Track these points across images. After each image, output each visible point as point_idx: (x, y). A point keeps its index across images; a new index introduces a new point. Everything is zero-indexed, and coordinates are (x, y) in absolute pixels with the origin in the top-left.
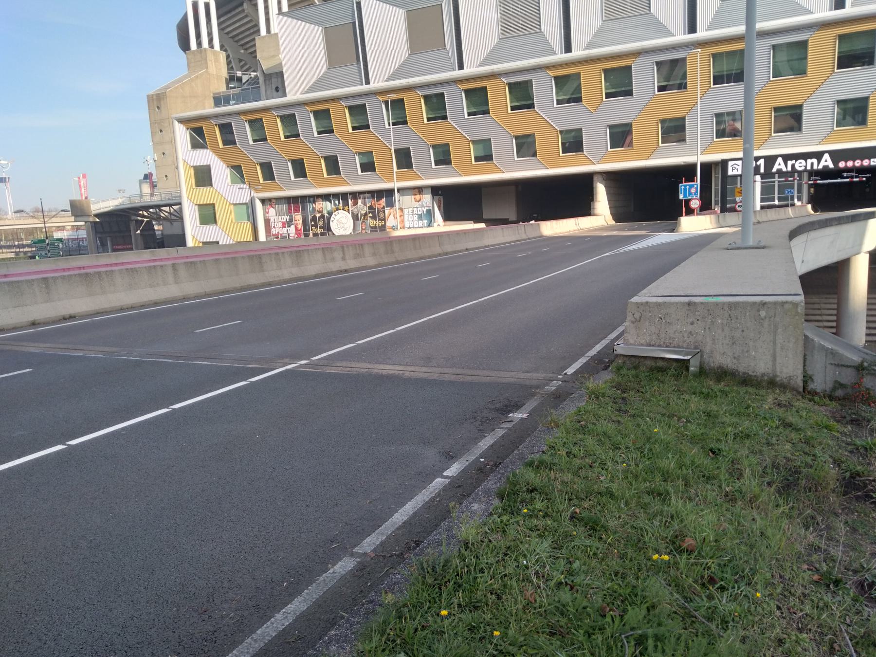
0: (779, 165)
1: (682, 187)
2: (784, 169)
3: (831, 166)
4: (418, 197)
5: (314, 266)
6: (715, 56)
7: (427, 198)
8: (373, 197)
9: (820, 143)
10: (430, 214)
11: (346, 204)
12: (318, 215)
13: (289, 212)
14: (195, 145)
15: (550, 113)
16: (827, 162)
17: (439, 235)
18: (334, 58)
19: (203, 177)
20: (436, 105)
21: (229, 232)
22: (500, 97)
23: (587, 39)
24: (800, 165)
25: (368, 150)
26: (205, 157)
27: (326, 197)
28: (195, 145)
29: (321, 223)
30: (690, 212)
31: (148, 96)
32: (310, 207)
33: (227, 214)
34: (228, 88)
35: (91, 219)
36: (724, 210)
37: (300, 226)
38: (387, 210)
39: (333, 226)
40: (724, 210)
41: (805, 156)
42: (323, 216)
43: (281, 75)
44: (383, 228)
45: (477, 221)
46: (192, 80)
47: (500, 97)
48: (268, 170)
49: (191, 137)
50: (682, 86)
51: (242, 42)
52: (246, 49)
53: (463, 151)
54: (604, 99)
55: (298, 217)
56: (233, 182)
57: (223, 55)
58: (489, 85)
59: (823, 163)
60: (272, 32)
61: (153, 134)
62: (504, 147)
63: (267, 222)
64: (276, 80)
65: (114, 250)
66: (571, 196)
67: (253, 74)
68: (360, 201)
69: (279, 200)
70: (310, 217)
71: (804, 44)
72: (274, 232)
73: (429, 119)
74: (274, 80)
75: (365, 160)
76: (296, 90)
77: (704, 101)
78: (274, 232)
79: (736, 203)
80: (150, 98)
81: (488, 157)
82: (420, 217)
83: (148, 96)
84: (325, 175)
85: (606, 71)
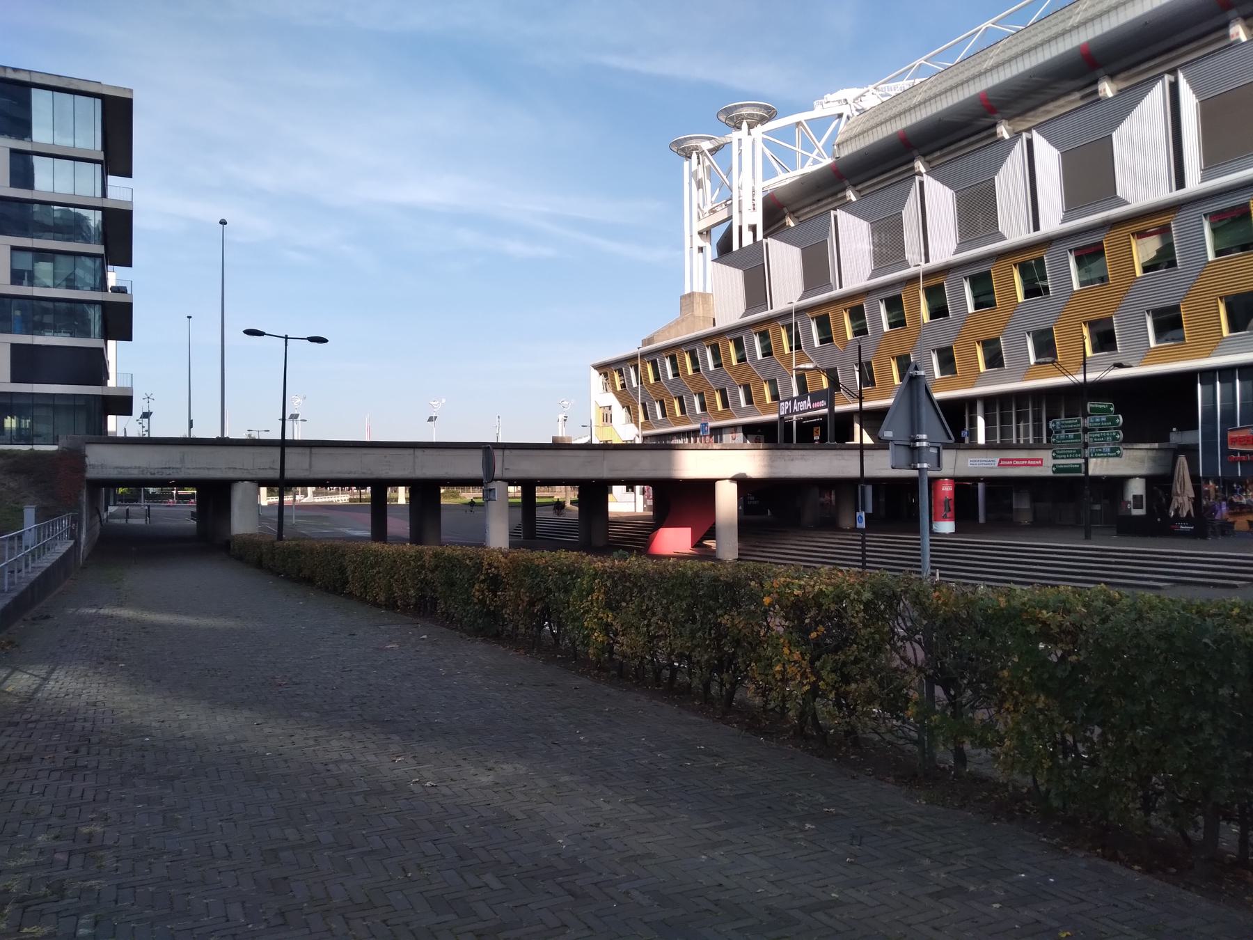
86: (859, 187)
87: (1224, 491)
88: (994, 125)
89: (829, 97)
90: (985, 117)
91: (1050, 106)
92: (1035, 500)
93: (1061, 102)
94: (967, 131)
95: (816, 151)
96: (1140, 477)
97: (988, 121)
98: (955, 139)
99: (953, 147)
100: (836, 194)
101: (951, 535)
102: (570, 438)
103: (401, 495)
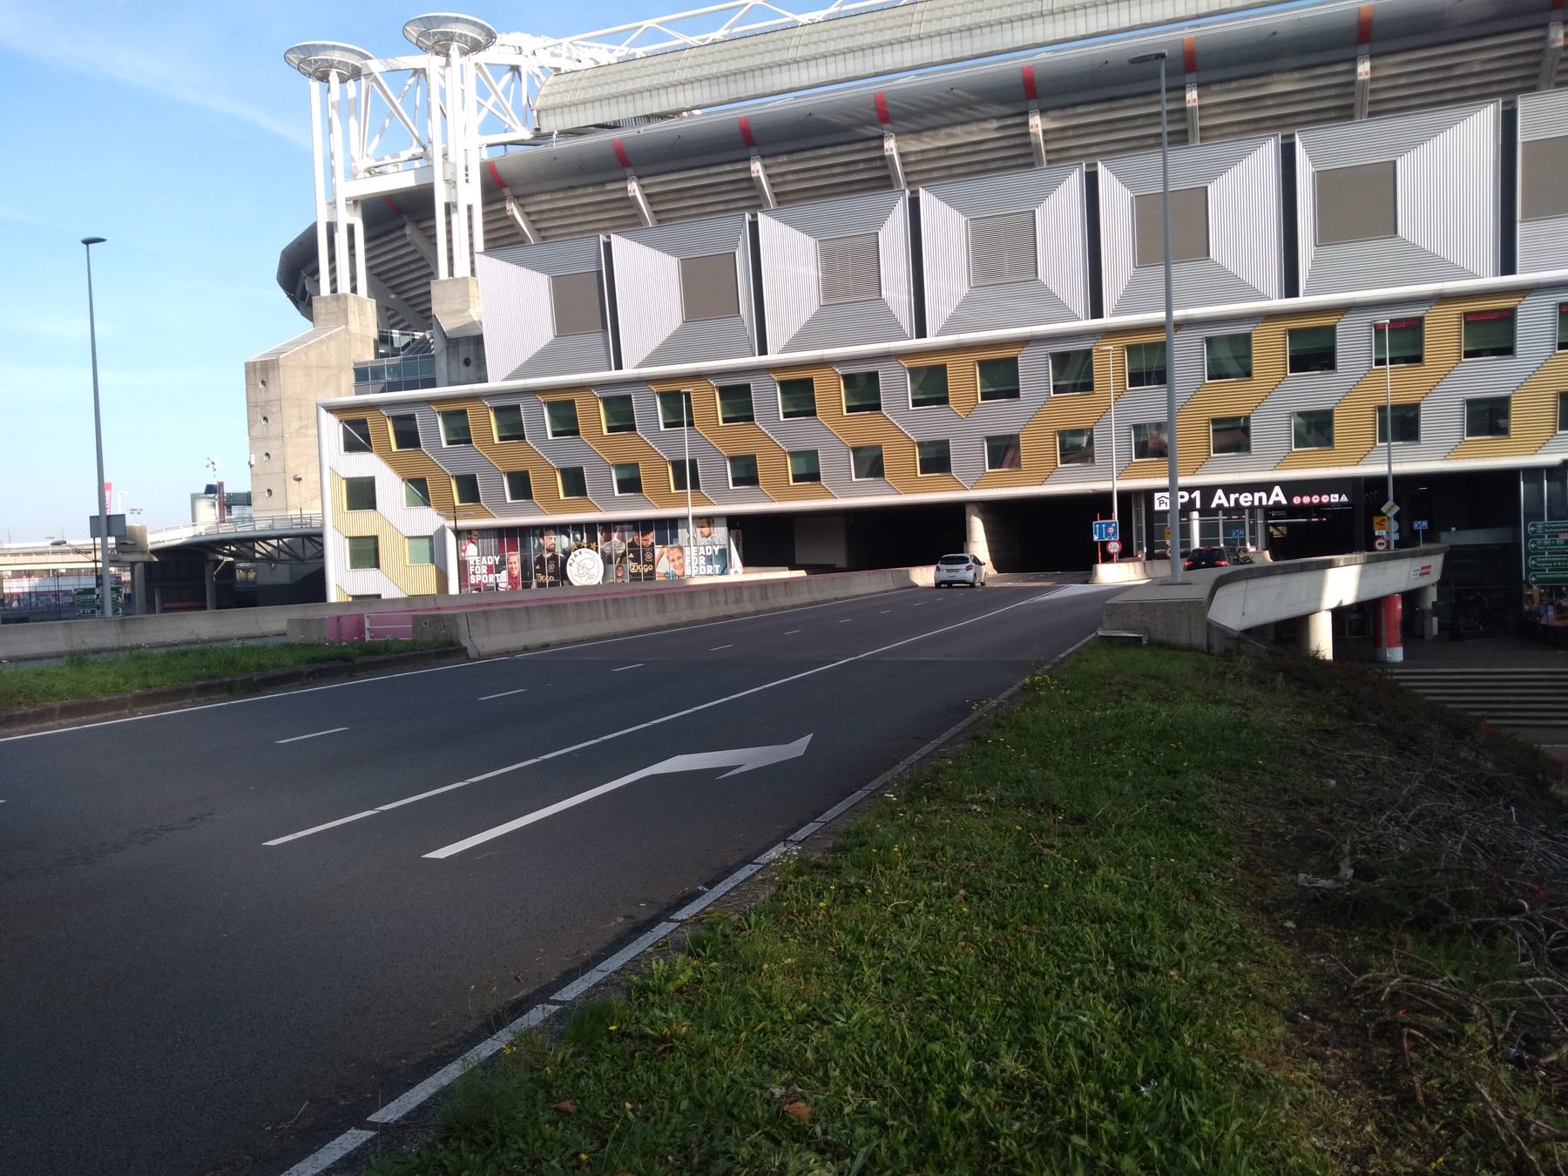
0: (1219, 499)
1: (1096, 525)
3: (1284, 502)
4: (706, 530)
5: (545, 632)
6: (1130, 348)
7: (720, 533)
8: (636, 530)
9: (1275, 469)
10: (724, 555)
11: (593, 539)
12: (547, 555)
13: (500, 551)
14: (351, 446)
15: (902, 420)
16: (1278, 496)
17: (738, 587)
18: (566, 321)
19: (362, 494)
20: (737, 400)
21: (399, 579)
22: (830, 394)
23: (948, 311)
24: (1245, 499)
25: (632, 461)
26: (366, 464)
27: (562, 529)
28: (351, 446)
29: (552, 567)
30: (1108, 558)
31: (247, 365)
32: (534, 543)
33: (395, 552)
34: (378, 355)
35: (146, 558)
36: (1151, 556)
37: (517, 571)
38: (658, 549)
39: (572, 571)
40: (1151, 556)
41: (1252, 487)
42: (554, 557)
43: (478, 341)
44: (651, 575)
45: (793, 567)
46: (321, 342)
47: (830, 394)
48: (469, 489)
49: (346, 431)
50: (1088, 387)
51: (394, 282)
52: (399, 294)
53: (776, 466)
55: (515, 559)
56: (411, 503)
57: (371, 305)
58: (818, 377)
59: (1273, 499)
60: (457, 274)
61: (251, 424)
62: (836, 461)
63: (463, 566)
64: (469, 350)
65: (165, 610)
66: (936, 532)
67: (418, 335)
68: (615, 536)
69: (484, 532)
70: (533, 559)
72: (473, 580)
73: (725, 420)
74: (462, 348)
75: (626, 475)
76: (502, 370)
77: (1117, 409)
78: (473, 580)
79: (1166, 547)
80: (250, 368)
81: (814, 476)
82: (709, 560)
83: (247, 365)
84: (562, 497)
85: (982, 364)
87: (1550, 595)
88: (881, 137)
90: (874, 125)
91: (958, 130)
93: (973, 127)
94: (844, 137)
95: (493, 98)
97: (873, 131)
98: (830, 152)
99: (808, 154)
100: (603, 183)
102: (143, 530)
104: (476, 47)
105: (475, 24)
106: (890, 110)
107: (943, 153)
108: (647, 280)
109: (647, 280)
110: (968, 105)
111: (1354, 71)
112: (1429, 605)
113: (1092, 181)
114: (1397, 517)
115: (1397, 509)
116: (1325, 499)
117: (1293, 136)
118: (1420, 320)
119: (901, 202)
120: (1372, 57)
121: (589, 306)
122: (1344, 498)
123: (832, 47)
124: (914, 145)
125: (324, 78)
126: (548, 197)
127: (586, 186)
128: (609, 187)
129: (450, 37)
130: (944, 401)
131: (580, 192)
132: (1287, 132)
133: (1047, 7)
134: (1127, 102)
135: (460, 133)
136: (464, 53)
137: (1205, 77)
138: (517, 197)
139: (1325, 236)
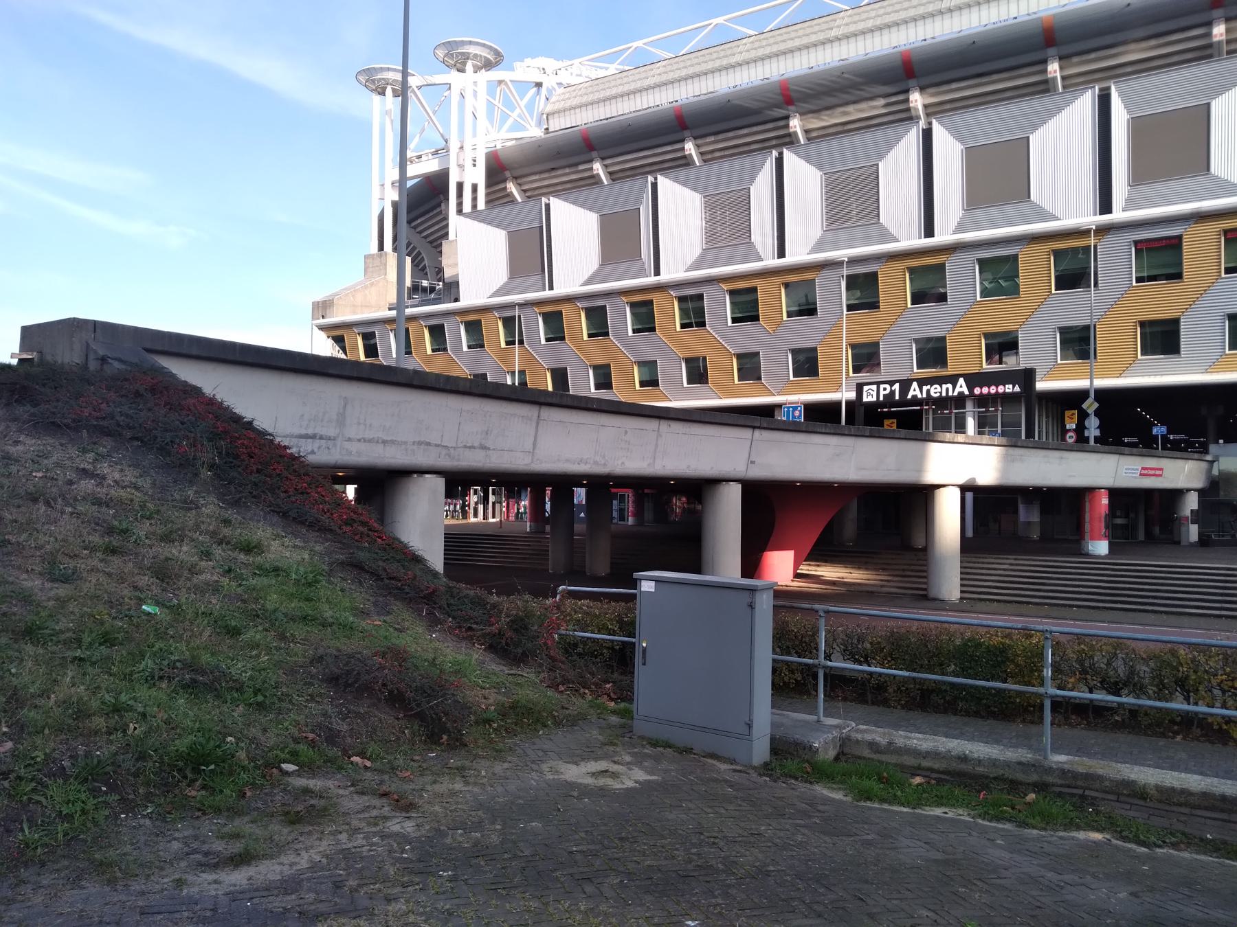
2: (919, 396)
3: (967, 392)
54: (909, 305)
59: (958, 389)
71: (874, 276)
76: (471, 296)
86: (608, 162)
88: (787, 118)
89: (528, 61)
91: (850, 108)
92: (1043, 512)
93: (863, 105)
95: (518, 111)
96: (1195, 490)
97: (783, 112)
98: (741, 126)
99: (730, 134)
100: (576, 165)
101: (1105, 557)
103: (580, 495)
104: (488, 65)
105: (484, 45)
106: (793, 95)
107: (840, 129)
108: (575, 230)
109: (575, 230)
110: (855, 86)
111: (1209, 35)
112: (1188, 513)
113: (927, 135)
114: (1097, 413)
115: (1096, 405)
116: (1001, 389)
117: (1109, 88)
118: (1179, 238)
119: (768, 161)
120: (1228, 20)
121: (531, 253)
122: (1017, 389)
123: (768, 51)
124: (815, 123)
125: (383, 93)
126: (537, 177)
127: (564, 167)
128: (581, 167)
129: (466, 57)
130: (756, 318)
131: (559, 172)
132: (1104, 85)
133: (945, 5)
134: (995, 77)
135: (473, 126)
136: (477, 69)
137: (1066, 50)
138: (515, 178)
139: (1139, 176)
